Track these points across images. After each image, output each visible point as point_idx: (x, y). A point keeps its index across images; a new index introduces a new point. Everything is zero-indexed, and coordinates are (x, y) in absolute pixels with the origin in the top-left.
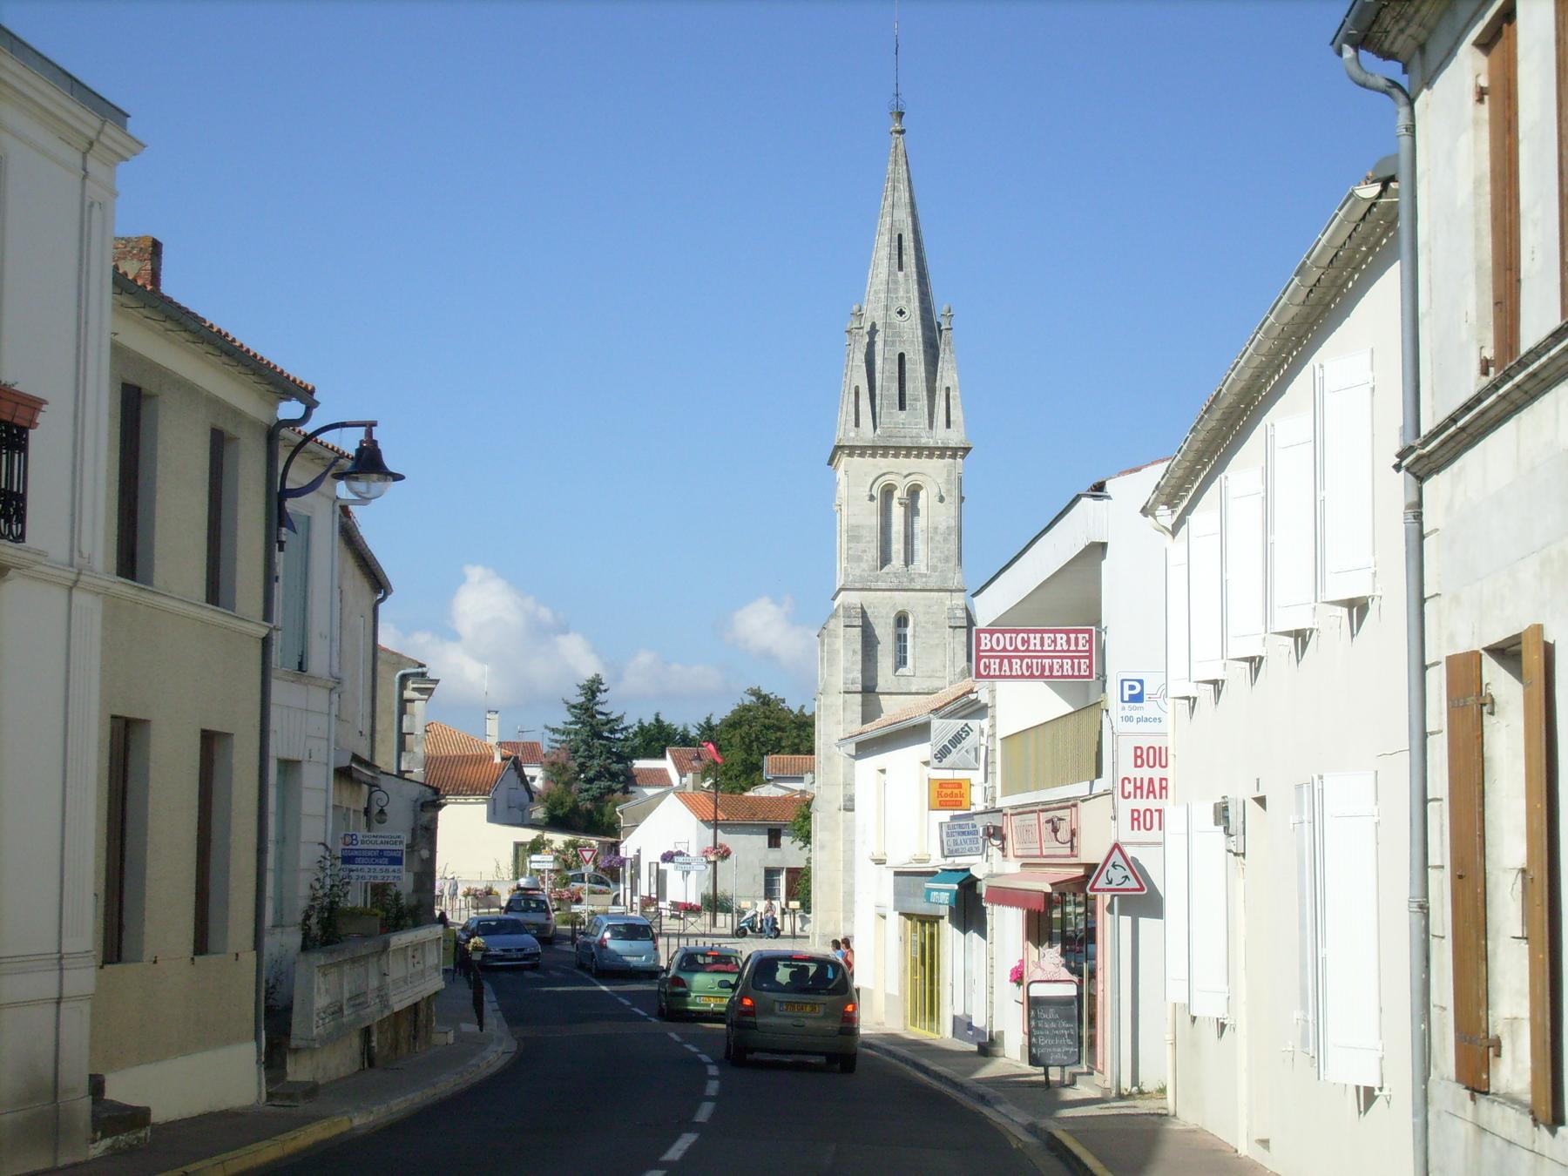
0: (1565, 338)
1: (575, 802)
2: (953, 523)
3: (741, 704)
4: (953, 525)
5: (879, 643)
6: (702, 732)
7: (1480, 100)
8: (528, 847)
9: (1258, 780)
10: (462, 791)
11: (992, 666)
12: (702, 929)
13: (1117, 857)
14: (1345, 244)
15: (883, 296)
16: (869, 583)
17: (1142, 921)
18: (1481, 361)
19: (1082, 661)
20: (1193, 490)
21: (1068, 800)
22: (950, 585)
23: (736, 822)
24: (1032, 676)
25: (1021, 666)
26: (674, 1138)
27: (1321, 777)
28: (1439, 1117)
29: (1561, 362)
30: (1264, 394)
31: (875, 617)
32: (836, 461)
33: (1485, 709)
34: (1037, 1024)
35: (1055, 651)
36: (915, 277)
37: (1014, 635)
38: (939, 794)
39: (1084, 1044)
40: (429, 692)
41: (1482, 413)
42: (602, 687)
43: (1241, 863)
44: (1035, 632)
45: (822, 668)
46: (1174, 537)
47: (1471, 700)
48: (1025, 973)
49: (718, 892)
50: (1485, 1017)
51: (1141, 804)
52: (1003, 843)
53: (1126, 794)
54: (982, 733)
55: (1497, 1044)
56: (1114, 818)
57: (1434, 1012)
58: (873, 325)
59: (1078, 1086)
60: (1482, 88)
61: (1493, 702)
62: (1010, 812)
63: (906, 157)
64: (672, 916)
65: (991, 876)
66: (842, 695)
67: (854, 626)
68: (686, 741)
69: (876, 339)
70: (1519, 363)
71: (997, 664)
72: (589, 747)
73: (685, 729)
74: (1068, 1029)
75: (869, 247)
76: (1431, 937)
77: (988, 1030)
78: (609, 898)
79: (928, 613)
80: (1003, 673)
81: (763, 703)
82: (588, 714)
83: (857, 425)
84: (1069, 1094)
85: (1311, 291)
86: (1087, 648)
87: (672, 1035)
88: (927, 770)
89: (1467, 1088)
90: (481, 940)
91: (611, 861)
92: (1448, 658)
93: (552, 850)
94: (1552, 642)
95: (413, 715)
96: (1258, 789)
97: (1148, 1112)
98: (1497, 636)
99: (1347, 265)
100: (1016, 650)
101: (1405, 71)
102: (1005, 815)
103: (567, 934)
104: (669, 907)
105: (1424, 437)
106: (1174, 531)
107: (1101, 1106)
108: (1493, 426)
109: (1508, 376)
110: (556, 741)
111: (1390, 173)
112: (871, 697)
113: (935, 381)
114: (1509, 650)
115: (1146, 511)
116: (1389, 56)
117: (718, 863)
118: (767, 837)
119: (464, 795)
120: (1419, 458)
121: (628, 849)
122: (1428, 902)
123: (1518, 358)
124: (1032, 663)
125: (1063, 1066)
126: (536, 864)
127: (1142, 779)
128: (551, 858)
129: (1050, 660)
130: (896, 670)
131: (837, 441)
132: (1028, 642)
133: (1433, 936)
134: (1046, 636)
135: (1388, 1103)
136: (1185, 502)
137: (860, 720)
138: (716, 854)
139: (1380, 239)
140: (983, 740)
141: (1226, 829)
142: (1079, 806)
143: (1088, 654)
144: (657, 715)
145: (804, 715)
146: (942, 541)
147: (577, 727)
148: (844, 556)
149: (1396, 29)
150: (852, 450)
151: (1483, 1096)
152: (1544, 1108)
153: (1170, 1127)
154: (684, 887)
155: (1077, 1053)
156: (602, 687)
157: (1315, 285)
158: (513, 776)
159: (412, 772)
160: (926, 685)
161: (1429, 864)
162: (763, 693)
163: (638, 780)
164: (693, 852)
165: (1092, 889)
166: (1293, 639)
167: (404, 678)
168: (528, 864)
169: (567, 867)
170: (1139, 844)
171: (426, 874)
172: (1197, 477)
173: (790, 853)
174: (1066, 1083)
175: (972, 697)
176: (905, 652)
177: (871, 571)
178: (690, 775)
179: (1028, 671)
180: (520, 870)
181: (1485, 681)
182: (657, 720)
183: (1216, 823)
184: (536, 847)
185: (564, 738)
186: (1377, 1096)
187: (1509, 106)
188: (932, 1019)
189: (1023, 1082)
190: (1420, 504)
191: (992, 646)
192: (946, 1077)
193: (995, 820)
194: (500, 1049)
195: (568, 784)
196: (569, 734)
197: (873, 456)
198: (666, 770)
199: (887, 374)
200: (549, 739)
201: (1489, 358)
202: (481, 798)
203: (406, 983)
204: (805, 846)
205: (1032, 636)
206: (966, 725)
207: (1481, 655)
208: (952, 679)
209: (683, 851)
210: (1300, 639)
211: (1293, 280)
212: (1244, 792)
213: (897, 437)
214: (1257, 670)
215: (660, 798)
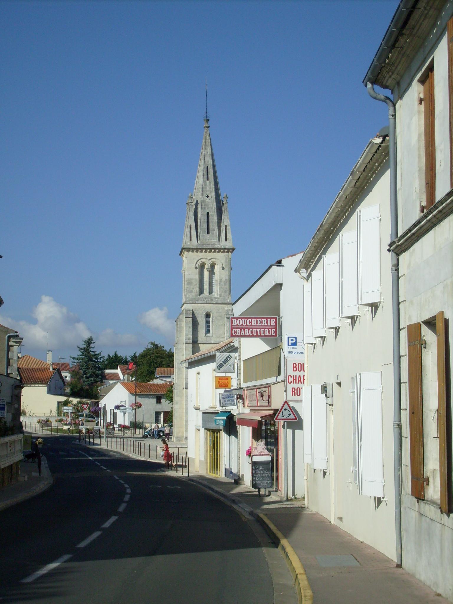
0: (452, 196)
1: (82, 386)
2: (228, 278)
3: (147, 348)
4: (228, 278)
5: (199, 324)
6: (132, 359)
7: (421, 103)
8: (63, 403)
9: (338, 375)
10: (37, 382)
11: (237, 332)
12: (130, 435)
13: (286, 406)
14: (369, 162)
15: (201, 190)
16: (195, 301)
17: (296, 431)
18: (421, 207)
19: (273, 330)
20: (314, 262)
21: (267, 384)
23: (144, 394)
24: (253, 336)
25: (249, 332)
26: (109, 518)
27: (360, 374)
28: (405, 510)
29: (451, 206)
30: (340, 223)
32: (182, 253)
33: (422, 346)
34: (255, 472)
35: (262, 326)
36: (213, 183)
37: (246, 320)
38: (219, 382)
39: (274, 480)
40: (19, 343)
41: (421, 228)
42: (93, 342)
43: (332, 408)
44: (254, 318)
45: (177, 334)
46: (307, 281)
47: (417, 343)
48: (252, 452)
49: (137, 420)
50: (423, 469)
51: (296, 386)
52: (243, 401)
53: (290, 382)
54: (236, 358)
55: (428, 480)
56: (285, 391)
57: (403, 467)
58: (197, 201)
59: (271, 496)
60: (421, 98)
61: (426, 343)
62: (246, 389)
63: (210, 137)
64: (119, 430)
65: (239, 414)
66: (185, 344)
67: (189, 318)
68: (126, 362)
69: (198, 207)
70: (434, 206)
71: (239, 331)
72: (87, 365)
73: (126, 358)
74: (268, 473)
75: (195, 171)
76: (402, 437)
77: (238, 474)
78: (95, 423)
80: (241, 335)
81: (156, 348)
82: (87, 352)
83: (191, 240)
84: (268, 499)
85: (357, 182)
86: (274, 325)
87: (115, 477)
88: (215, 373)
89: (416, 498)
90: (42, 439)
91: (95, 409)
92: (408, 326)
93: (72, 405)
94: (448, 319)
95: (13, 352)
96: (338, 379)
97: (298, 506)
98: (427, 316)
99: (370, 171)
100: (247, 325)
101: (392, 93)
102: (244, 390)
103: (77, 437)
104: (118, 427)
105: (399, 238)
106: (307, 279)
107: (280, 504)
108: (425, 232)
109: (430, 212)
110: (75, 362)
111: (386, 134)
112: (196, 345)
113: (221, 223)
114: (432, 322)
115: (296, 271)
116: (385, 87)
117: (137, 409)
118: (156, 399)
119: (38, 383)
120: (397, 246)
121: (101, 404)
122: (401, 423)
123: (434, 204)
124: (253, 331)
125: (265, 488)
126: (66, 410)
127: (296, 376)
128: (72, 408)
129: (260, 330)
130: (206, 334)
131: (183, 246)
132: (251, 322)
133: (403, 437)
134: (258, 320)
135: (386, 503)
136: (311, 267)
137: (192, 354)
138: (136, 406)
139: (383, 161)
140: (236, 361)
141: (326, 395)
142: (271, 386)
143: (275, 327)
144: (116, 352)
145: (171, 352)
146: (223, 285)
147: (83, 357)
148: (185, 290)
149: (388, 76)
150: (188, 250)
151: (422, 501)
152: (445, 506)
153: (305, 512)
154: (124, 419)
155: (271, 483)
156: (93, 342)
157: (358, 179)
158: (57, 375)
159: (12, 374)
160: (217, 340)
161: (402, 408)
162: (156, 344)
163: (107, 377)
164: (127, 405)
165: (276, 419)
166: (350, 320)
167: (9, 337)
168: (63, 410)
169: (78, 412)
170: (295, 401)
171: (18, 413)
172: (315, 257)
173: (165, 405)
174: (267, 494)
175: (232, 344)
176: (209, 327)
177: (196, 296)
178: (126, 376)
179: (251, 334)
180: (60, 413)
181: (423, 334)
182: (116, 354)
183: (322, 393)
184: (66, 403)
185: (78, 361)
186: (382, 501)
187: (431, 105)
188: (217, 470)
189: (250, 494)
190: (398, 265)
191: (237, 324)
192: (220, 493)
193: (240, 392)
194: (46, 483)
195: (79, 379)
196: (80, 359)
197: (197, 252)
198: (118, 374)
199: (202, 220)
200: (72, 361)
201: (424, 206)
202: (44, 385)
203: (7, 457)
204: (171, 403)
205: (253, 320)
206: (230, 355)
207: (421, 324)
208: (227, 338)
209: (123, 405)
210: (353, 320)
211: (349, 177)
212: (334, 381)
213: (206, 244)
214: (338, 332)
215: (115, 384)
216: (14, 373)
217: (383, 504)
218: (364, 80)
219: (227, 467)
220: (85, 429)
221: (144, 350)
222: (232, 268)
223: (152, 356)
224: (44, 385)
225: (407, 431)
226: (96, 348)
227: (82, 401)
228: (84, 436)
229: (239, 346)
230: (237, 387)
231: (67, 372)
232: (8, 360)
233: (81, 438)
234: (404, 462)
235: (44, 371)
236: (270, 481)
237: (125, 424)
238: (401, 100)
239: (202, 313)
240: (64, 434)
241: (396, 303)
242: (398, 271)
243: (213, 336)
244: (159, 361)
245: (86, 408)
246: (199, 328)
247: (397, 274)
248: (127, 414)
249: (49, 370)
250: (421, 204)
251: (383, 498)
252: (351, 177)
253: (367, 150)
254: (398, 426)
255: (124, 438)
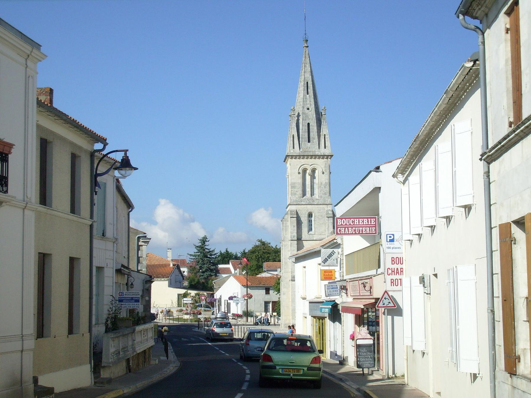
1: (198, 279)
2: (327, 181)
3: (255, 245)
4: (327, 182)
7: (507, 33)
9: (434, 268)
10: (159, 277)
11: (342, 230)
12: (243, 323)
15: (302, 103)
16: (299, 203)
17: (395, 317)
18: (509, 122)
19: (373, 228)
20: (410, 169)
21: (369, 276)
22: (327, 203)
24: (356, 234)
25: (352, 230)
27: (456, 267)
30: (434, 135)
31: (301, 214)
33: (513, 242)
36: (313, 97)
37: (349, 220)
38: (324, 275)
39: (376, 361)
41: (510, 140)
44: (357, 218)
46: (404, 185)
48: (355, 336)
51: (394, 277)
52: (347, 291)
53: (389, 274)
54: (339, 253)
55: (519, 358)
57: (497, 347)
58: (299, 113)
59: (374, 375)
60: (507, 28)
61: (515, 240)
62: (349, 280)
64: (232, 319)
65: (343, 303)
67: (294, 217)
68: (236, 258)
72: (203, 261)
74: (370, 355)
76: (495, 321)
79: (319, 212)
80: (345, 233)
83: (294, 148)
84: (371, 378)
85: (450, 99)
86: (374, 224)
88: (320, 266)
89: (509, 373)
91: (211, 300)
96: (434, 271)
98: (516, 217)
100: (350, 224)
101: (481, 23)
103: (196, 325)
104: (231, 315)
106: (404, 183)
107: (382, 381)
109: (518, 127)
110: (192, 259)
113: (320, 132)
115: (394, 176)
116: (475, 18)
119: (160, 278)
121: (217, 295)
122: (494, 309)
123: (522, 121)
124: (356, 229)
125: (369, 368)
129: (362, 228)
132: (354, 222)
133: (496, 321)
135: (481, 379)
136: (407, 173)
140: (339, 256)
141: (424, 285)
143: (375, 226)
144: (227, 249)
145: (277, 248)
146: (323, 187)
148: (290, 193)
149: (478, 8)
150: (292, 157)
151: (514, 376)
154: (236, 309)
155: (374, 363)
156: (207, 240)
157: (451, 97)
158: (177, 270)
159: (142, 270)
161: (494, 296)
164: (239, 296)
166: (446, 219)
167: (139, 238)
169: (196, 303)
170: (394, 291)
171: (148, 305)
173: (273, 296)
175: (335, 241)
176: (312, 226)
179: (354, 232)
180: (180, 303)
182: (227, 251)
184: (185, 295)
185: (194, 257)
186: (478, 377)
189: (355, 374)
190: (489, 172)
193: (344, 284)
197: (299, 158)
198: (230, 268)
201: (512, 121)
202: (166, 279)
203: (141, 342)
204: (278, 293)
205: (355, 220)
206: (333, 251)
209: (236, 296)
210: (448, 219)
214: (433, 230)
215: (228, 277)
216: (143, 270)
217: (478, 379)
218: (456, 13)
219: (332, 350)
220: (203, 318)
221: (252, 247)
222: (331, 172)
223: (260, 252)
224: (165, 280)
225: (499, 315)
226: (210, 246)
227: (200, 293)
228: (202, 324)
229: (341, 242)
230: (341, 279)
231: (185, 268)
232: (138, 258)
233: (200, 326)
234: (497, 342)
235: (165, 267)
236: (372, 362)
237: (238, 313)
238: (489, 29)
239: (305, 213)
240: (185, 323)
241: (487, 205)
242: (489, 177)
243: (315, 233)
244: (266, 257)
245: (204, 299)
246: (302, 227)
247: (488, 181)
248: (239, 305)
249: (169, 266)
250: (509, 120)
251: (478, 374)
252: (445, 95)
253: (459, 72)
254: (491, 311)
255: (238, 325)
